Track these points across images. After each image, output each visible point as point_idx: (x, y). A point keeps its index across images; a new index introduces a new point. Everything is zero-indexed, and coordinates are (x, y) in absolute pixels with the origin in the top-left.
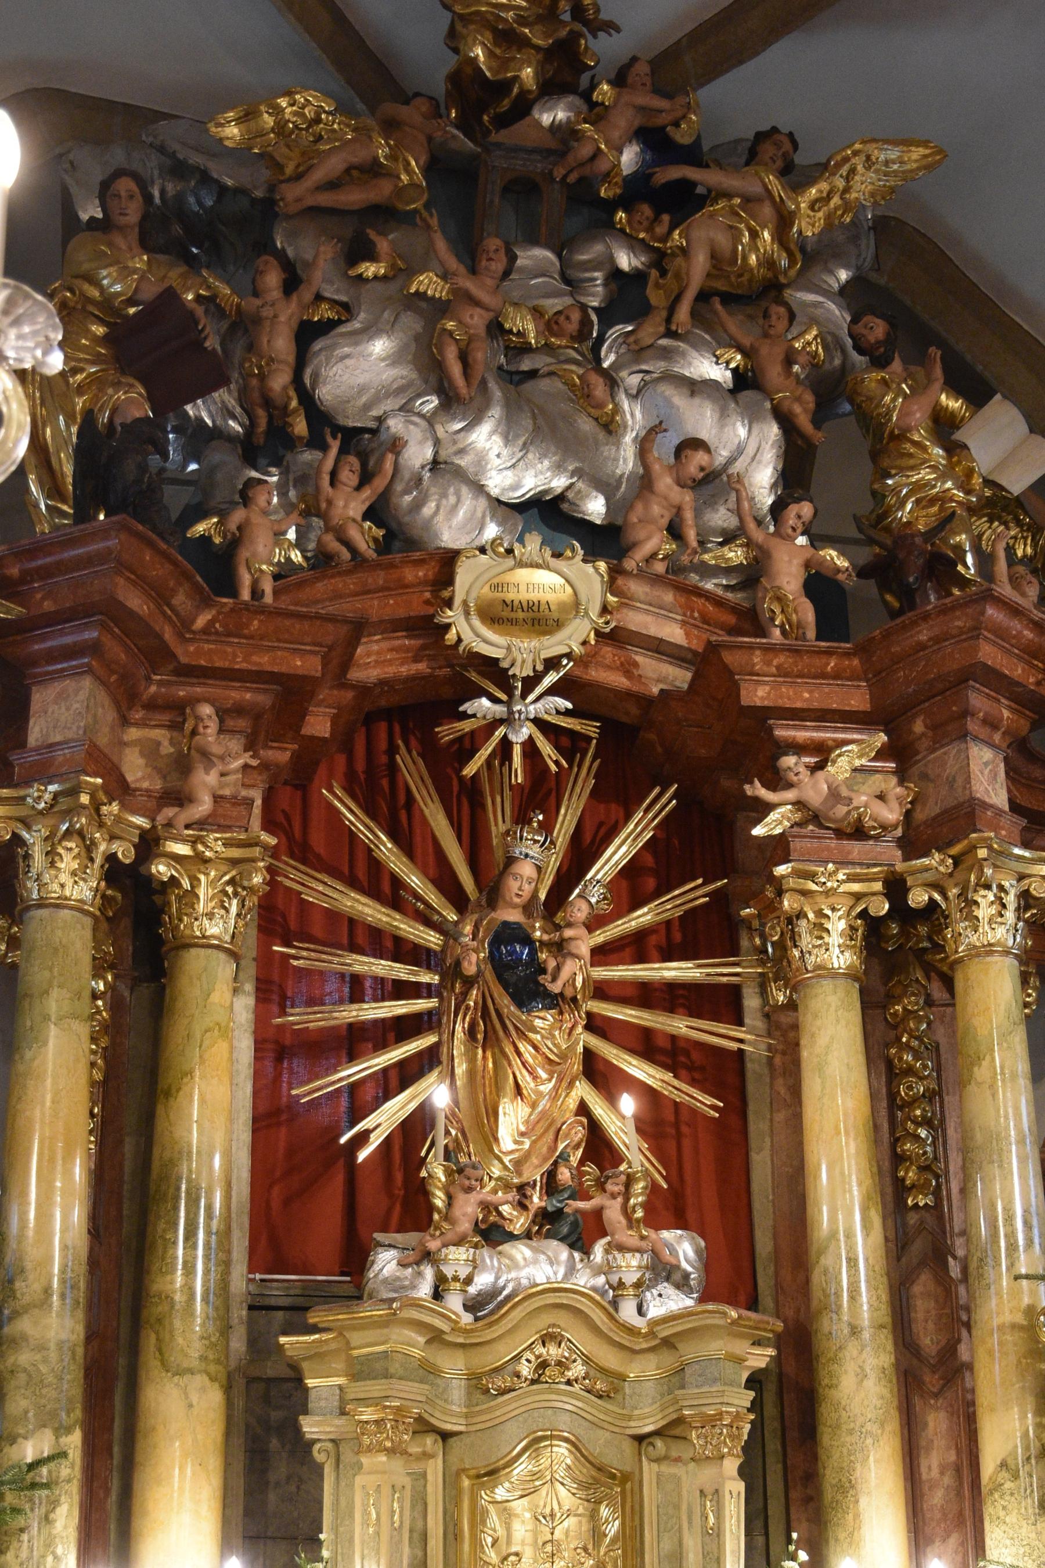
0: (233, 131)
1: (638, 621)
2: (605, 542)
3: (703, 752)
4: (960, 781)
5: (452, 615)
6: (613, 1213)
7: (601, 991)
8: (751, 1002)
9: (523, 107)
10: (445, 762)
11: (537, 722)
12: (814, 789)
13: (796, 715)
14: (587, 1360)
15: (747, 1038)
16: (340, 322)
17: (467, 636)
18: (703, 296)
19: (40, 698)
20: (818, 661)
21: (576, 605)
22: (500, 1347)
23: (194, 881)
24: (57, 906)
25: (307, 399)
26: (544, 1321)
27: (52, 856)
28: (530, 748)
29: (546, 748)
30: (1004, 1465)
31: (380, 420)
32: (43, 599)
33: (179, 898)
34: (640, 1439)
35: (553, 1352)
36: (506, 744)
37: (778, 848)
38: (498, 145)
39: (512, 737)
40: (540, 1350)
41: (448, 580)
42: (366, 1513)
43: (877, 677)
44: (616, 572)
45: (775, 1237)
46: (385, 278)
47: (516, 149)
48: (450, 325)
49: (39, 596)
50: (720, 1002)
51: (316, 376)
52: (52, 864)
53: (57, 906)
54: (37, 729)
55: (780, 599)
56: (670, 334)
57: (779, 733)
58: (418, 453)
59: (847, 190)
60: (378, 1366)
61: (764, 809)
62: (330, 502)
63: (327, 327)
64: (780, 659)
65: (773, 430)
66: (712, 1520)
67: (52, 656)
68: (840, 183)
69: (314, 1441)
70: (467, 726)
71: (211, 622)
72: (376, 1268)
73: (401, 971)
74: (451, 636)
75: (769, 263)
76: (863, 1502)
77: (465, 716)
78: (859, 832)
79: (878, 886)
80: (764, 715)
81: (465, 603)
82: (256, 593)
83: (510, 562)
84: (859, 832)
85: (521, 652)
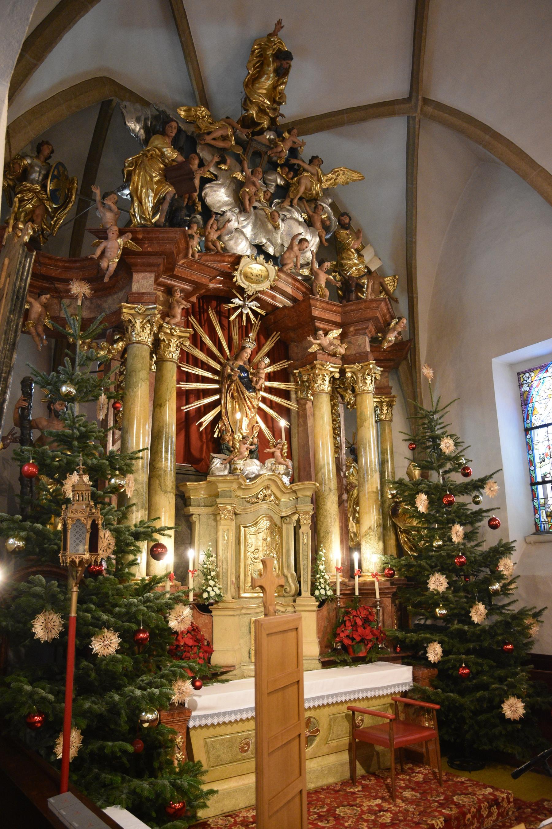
0: (183, 113)
1: (282, 285)
2: (276, 260)
3: (290, 324)
4: (363, 346)
5: (237, 274)
6: (278, 453)
7: (270, 390)
8: (293, 396)
9: (261, 132)
10: (223, 316)
11: (250, 308)
12: (325, 341)
13: (322, 320)
14: (275, 496)
15: (293, 405)
16: (214, 180)
17: (239, 280)
18: (301, 199)
19: (136, 276)
20: (331, 307)
21: (267, 277)
22: (254, 490)
23: (169, 340)
24: (143, 344)
25: (202, 200)
26: (266, 483)
27: (143, 328)
28: (247, 314)
29: (252, 316)
30: (370, 528)
31: (224, 212)
32: (148, 247)
33: (165, 346)
34: (282, 517)
35: (268, 492)
36: (241, 314)
37: (314, 355)
38: (255, 140)
39: (244, 311)
40: (264, 491)
41: (238, 263)
42: (223, 536)
43: (344, 314)
44: (280, 270)
45: (299, 462)
46: (226, 170)
47: (259, 143)
48: (247, 190)
49: (146, 246)
50: (285, 394)
51: (206, 195)
52: (143, 331)
53: (143, 344)
54: (135, 286)
55: (321, 287)
56: (291, 206)
57: (317, 324)
58: (234, 224)
59: (336, 179)
60: (228, 494)
61: (311, 344)
62: (209, 233)
63: (209, 181)
64: (323, 305)
65: (318, 239)
66: (305, 541)
67: (143, 265)
68: (334, 176)
69: (193, 514)
70: (232, 306)
71: (183, 263)
72: (214, 464)
73: (209, 375)
74: (235, 280)
75: (317, 194)
76: (333, 536)
77: (232, 303)
78: (334, 355)
79: (338, 370)
80: (315, 318)
81: (241, 271)
82: (193, 256)
83: (255, 262)
84: (334, 355)
85: (251, 288)
